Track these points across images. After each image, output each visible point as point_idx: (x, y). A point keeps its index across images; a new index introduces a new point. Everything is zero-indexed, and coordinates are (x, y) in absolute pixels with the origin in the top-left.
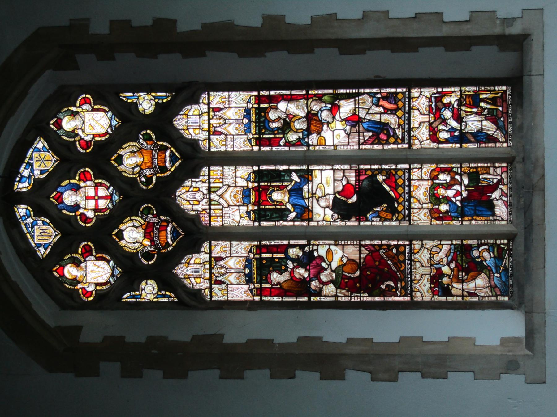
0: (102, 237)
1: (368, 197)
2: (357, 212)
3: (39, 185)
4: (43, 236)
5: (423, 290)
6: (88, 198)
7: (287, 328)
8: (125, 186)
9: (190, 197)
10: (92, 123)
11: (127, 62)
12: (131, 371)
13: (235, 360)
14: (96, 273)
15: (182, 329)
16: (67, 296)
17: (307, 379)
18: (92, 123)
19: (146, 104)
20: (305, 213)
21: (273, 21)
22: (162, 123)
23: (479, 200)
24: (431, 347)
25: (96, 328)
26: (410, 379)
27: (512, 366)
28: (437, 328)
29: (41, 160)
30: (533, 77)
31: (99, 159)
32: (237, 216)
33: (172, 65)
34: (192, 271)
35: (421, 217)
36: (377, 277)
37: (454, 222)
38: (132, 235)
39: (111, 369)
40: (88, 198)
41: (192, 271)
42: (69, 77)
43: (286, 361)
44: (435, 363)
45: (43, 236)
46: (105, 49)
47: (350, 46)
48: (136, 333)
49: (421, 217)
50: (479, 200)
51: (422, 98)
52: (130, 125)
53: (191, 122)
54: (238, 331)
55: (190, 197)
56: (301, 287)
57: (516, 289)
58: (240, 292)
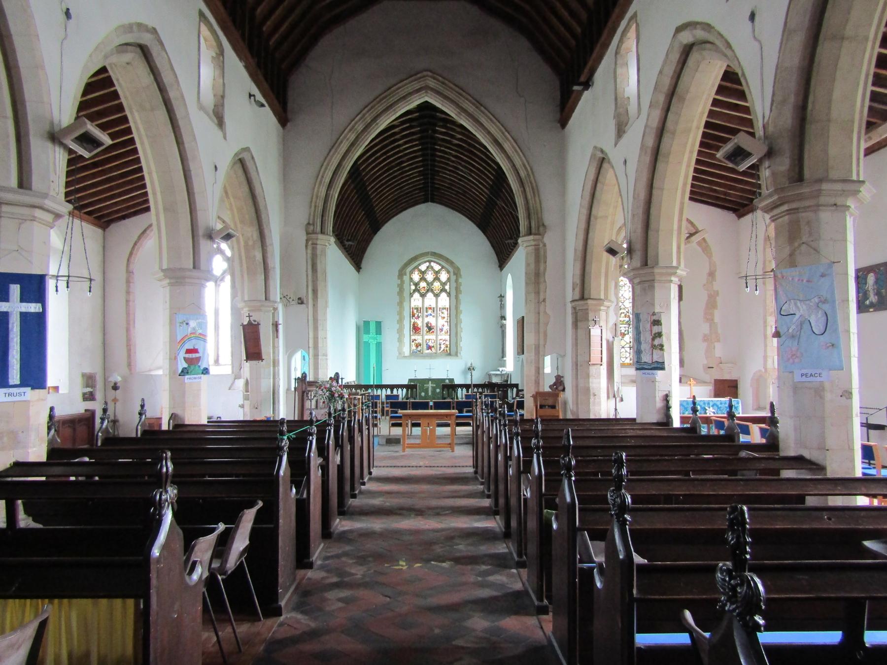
0: (423, 279)
1: (430, 328)
2: (427, 326)
3: (432, 268)
4: (423, 267)
5: (413, 337)
6: (430, 277)
7: (406, 314)
8: (432, 283)
9: (430, 295)
10: (444, 276)
11: (454, 285)
12: (398, 285)
13: (401, 304)
14: (416, 277)
15: (406, 294)
16: (411, 272)
17: (397, 317)
18: (444, 276)
19: (447, 287)
20: (427, 316)
21: (461, 312)
22: (443, 290)
23: (429, 348)
24: (255, 174)
25: (406, 278)
26: (397, 336)
27: (400, 353)
28: (406, 340)
29: (437, 267)
30: (589, 302)
31: (437, 279)
32: (426, 305)
33: (453, 294)
34: (416, 295)
35: (426, 337)
36: (416, 329)
37: (444, 564)
38: (423, 284)
39: (399, 282)
40: (430, 277)
41: (416, 295)
42: (452, 274)
43: (400, 314)
44: (400, 340)
45: (423, 267)
46: (456, 281)
47: (456, 325)
48: (406, 286)
49: (426, 337)
50: (429, 348)
51: (447, 337)
52: (443, 284)
53: (444, 295)
54: (406, 305)
55: (430, 295)
56: (413, 316)
57: (414, 354)
58: (412, 306)
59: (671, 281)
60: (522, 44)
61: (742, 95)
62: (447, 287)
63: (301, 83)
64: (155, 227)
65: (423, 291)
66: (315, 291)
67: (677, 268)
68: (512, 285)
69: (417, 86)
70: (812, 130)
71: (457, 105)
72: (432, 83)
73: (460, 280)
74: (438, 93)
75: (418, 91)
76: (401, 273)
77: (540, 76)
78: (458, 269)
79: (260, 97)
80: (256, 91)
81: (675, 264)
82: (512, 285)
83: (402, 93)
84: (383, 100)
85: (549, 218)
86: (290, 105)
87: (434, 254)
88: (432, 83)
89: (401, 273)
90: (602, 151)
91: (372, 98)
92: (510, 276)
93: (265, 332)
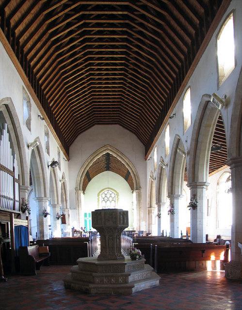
4: (106, 193)
6: (108, 196)
14: (104, 196)
18: (113, 195)
19: (114, 199)
25: (100, 196)
29: (111, 193)
38: (106, 198)
40: (108, 196)
59: (203, 188)
60: (134, 136)
61: (223, 127)
62: (114, 199)
63: (72, 148)
64: (34, 190)
65: (106, 200)
66: (78, 206)
67: (205, 183)
68: (135, 194)
69: (105, 149)
70: (173, 186)
71: (117, 154)
72: (109, 148)
73: (119, 197)
74: (110, 150)
75: (105, 150)
76: (98, 195)
77: (140, 146)
78: (118, 193)
79: (66, 159)
80: (65, 158)
81: (180, 194)
82: (135, 194)
83: (101, 151)
84: (96, 153)
85: (142, 185)
86: (70, 155)
87: (108, 188)
88: (109, 148)
89: (98, 195)
90: (178, 135)
91: (94, 151)
92: (168, 129)
93: (67, 216)
